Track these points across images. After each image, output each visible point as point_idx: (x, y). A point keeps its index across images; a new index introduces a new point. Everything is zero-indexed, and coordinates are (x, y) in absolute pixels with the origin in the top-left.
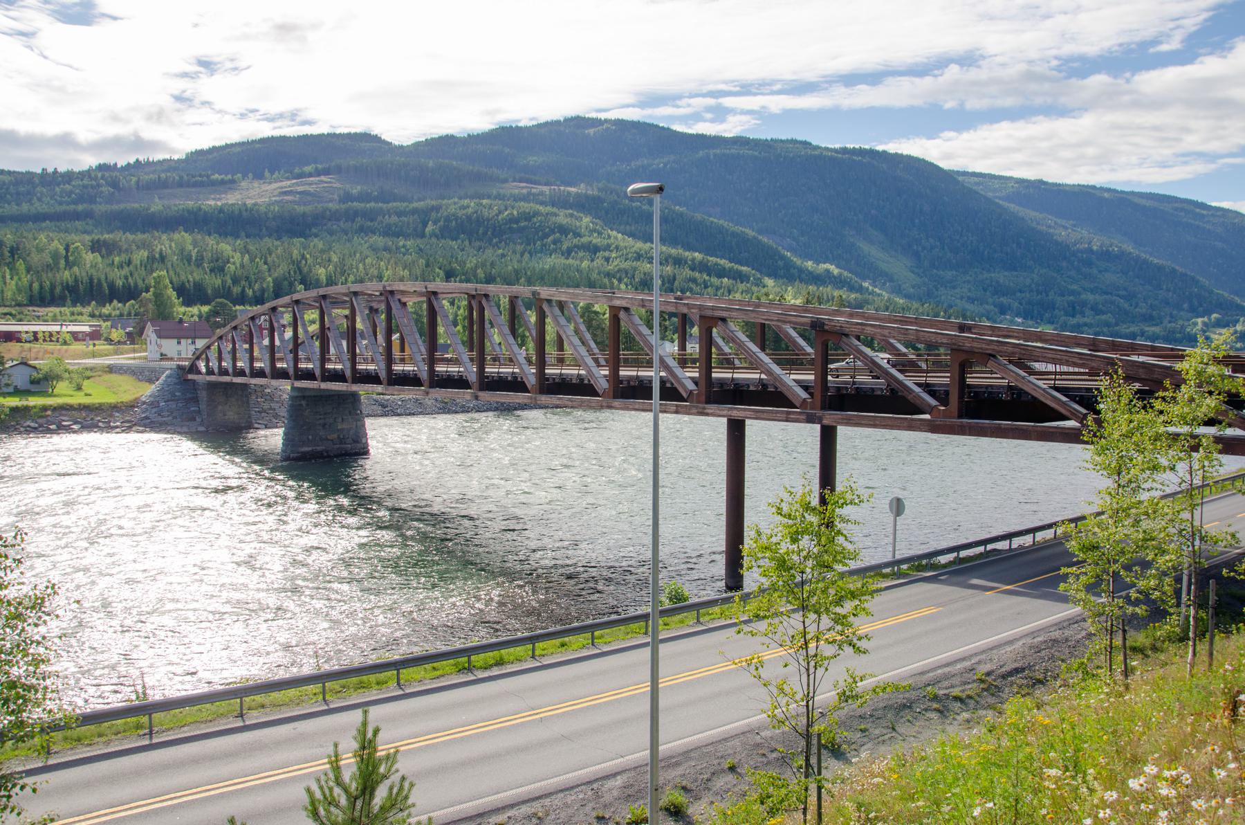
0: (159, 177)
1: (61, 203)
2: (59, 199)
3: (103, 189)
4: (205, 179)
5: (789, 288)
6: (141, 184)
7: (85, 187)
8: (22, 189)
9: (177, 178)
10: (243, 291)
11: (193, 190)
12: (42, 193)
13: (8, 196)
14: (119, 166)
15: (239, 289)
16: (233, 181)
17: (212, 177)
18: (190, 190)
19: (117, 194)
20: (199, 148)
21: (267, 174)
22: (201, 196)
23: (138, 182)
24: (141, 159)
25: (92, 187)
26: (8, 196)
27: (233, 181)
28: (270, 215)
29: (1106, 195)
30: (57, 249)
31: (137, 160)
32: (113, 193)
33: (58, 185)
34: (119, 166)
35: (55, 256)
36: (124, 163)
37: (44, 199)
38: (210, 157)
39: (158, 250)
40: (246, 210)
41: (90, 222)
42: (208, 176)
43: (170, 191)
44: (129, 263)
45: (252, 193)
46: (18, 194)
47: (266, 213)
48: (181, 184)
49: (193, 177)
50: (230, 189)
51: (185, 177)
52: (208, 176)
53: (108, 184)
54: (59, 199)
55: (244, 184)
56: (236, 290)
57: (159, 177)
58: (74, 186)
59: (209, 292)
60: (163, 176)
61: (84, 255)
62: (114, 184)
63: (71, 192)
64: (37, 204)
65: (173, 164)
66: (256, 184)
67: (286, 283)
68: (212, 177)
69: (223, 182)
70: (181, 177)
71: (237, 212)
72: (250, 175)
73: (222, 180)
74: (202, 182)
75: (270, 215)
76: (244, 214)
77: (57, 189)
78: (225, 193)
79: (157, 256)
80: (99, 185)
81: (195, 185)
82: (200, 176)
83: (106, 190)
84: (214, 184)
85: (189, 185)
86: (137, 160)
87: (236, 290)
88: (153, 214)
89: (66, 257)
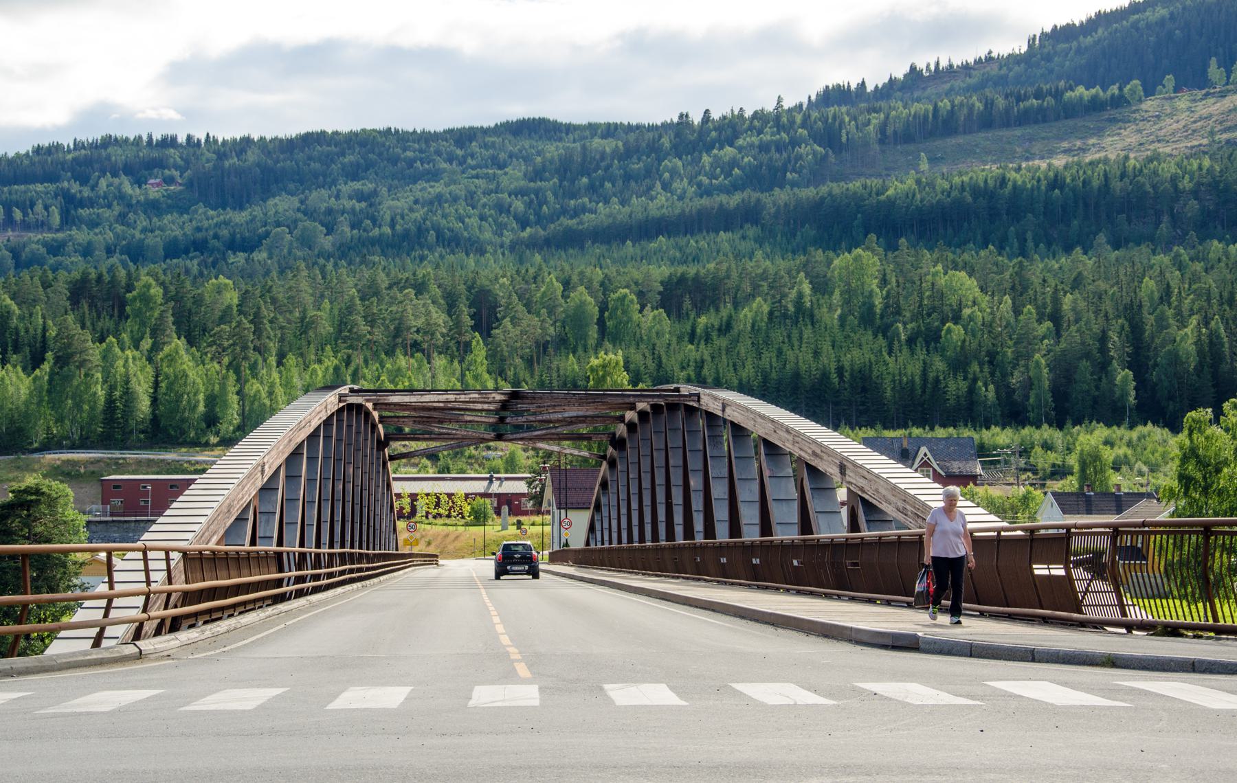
0: (936, 109)
1: (706, 192)
2: (705, 180)
3: (802, 150)
4: (1050, 101)
5: (903, 241)
6: (890, 130)
7: (764, 148)
8: (636, 166)
9: (979, 106)
10: (972, 390)
11: (1018, 132)
12: (674, 172)
13: (608, 185)
14: (870, 88)
15: (964, 386)
16: (1119, 102)
17: (1069, 95)
18: (1005, 133)
19: (832, 158)
20: (1062, 21)
21: (1215, 71)
22: (1037, 147)
23: (882, 128)
24: (921, 65)
25: (780, 147)
26: (608, 185)
27: (1119, 102)
28: (1186, 184)
29: (597, 143)
30: (583, 304)
31: (913, 68)
32: (825, 157)
33: (709, 148)
34: (870, 88)
35: (577, 319)
36: (882, 80)
37: (677, 185)
38: (1089, 40)
39: (793, 294)
40: (1123, 175)
41: (751, 231)
42: (1058, 94)
43: (960, 140)
44: (726, 328)
45: (1169, 126)
46: (628, 177)
47: (1174, 179)
48: (987, 121)
49: (1019, 99)
50: (1113, 120)
51: (1001, 102)
52: (1058, 94)
53: (816, 138)
54: (705, 180)
55: (1150, 105)
56: (955, 387)
57: (936, 109)
58: (740, 149)
59: (889, 393)
60: (945, 104)
61: (636, 316)
62: (829, 136)
63: (734, 163)
64: (662, 199)
65: (994, 70)
66: (1183, 102)
67: (1085, 364)
68: (1069, 95)
69: (1095, 106)
70: (989, 104)
71: (1096, 183)
72: (1169, 81)
73: (1094, 98)
74: (1040, 109)
75: (1186, 184)
76: (1117, 185)
77: (706, 159)
78: (1099, 132)
79: (791, 308)
80: (795, 143)
81: (1025, 118)
82: (1038, 95)
83: (809, 151)
84: (1071, 111)
85: (1008, 121)
86: (913, 68)
87: (955, 387)
88: (891, 202)
89: (601, 322)
